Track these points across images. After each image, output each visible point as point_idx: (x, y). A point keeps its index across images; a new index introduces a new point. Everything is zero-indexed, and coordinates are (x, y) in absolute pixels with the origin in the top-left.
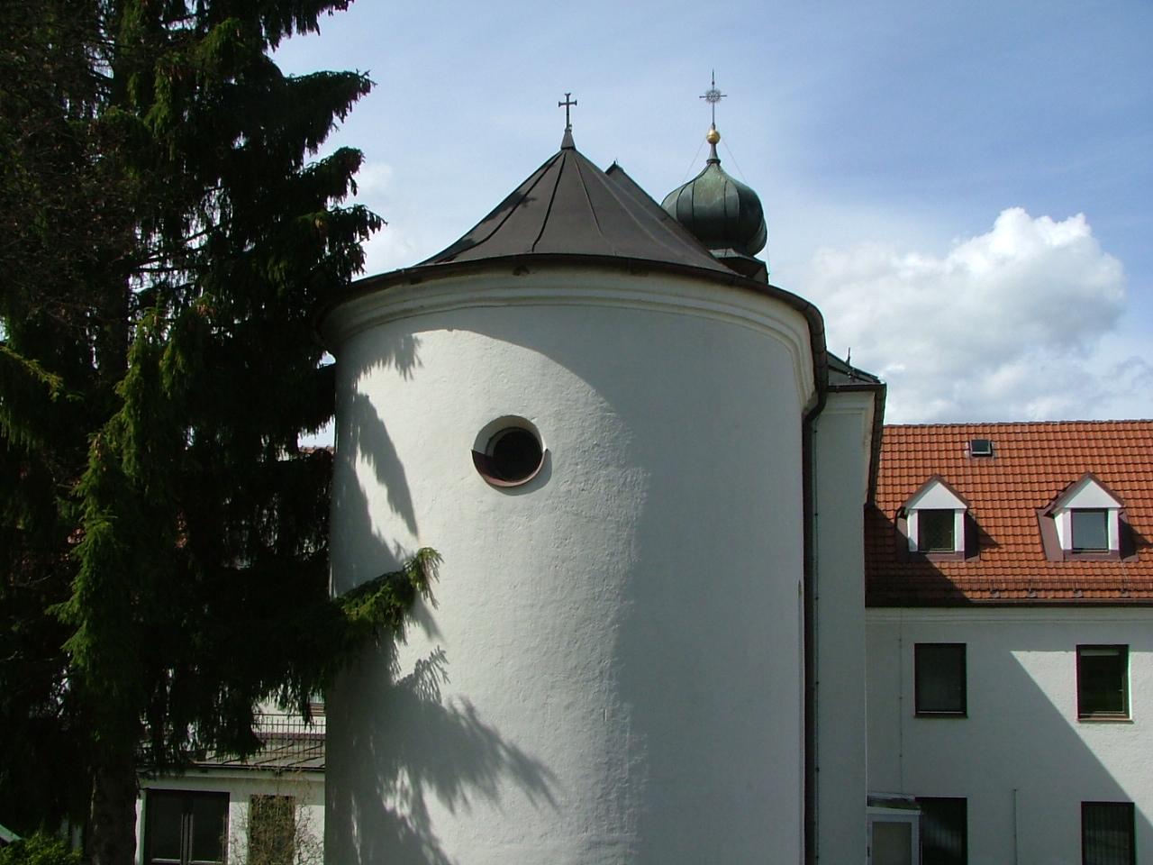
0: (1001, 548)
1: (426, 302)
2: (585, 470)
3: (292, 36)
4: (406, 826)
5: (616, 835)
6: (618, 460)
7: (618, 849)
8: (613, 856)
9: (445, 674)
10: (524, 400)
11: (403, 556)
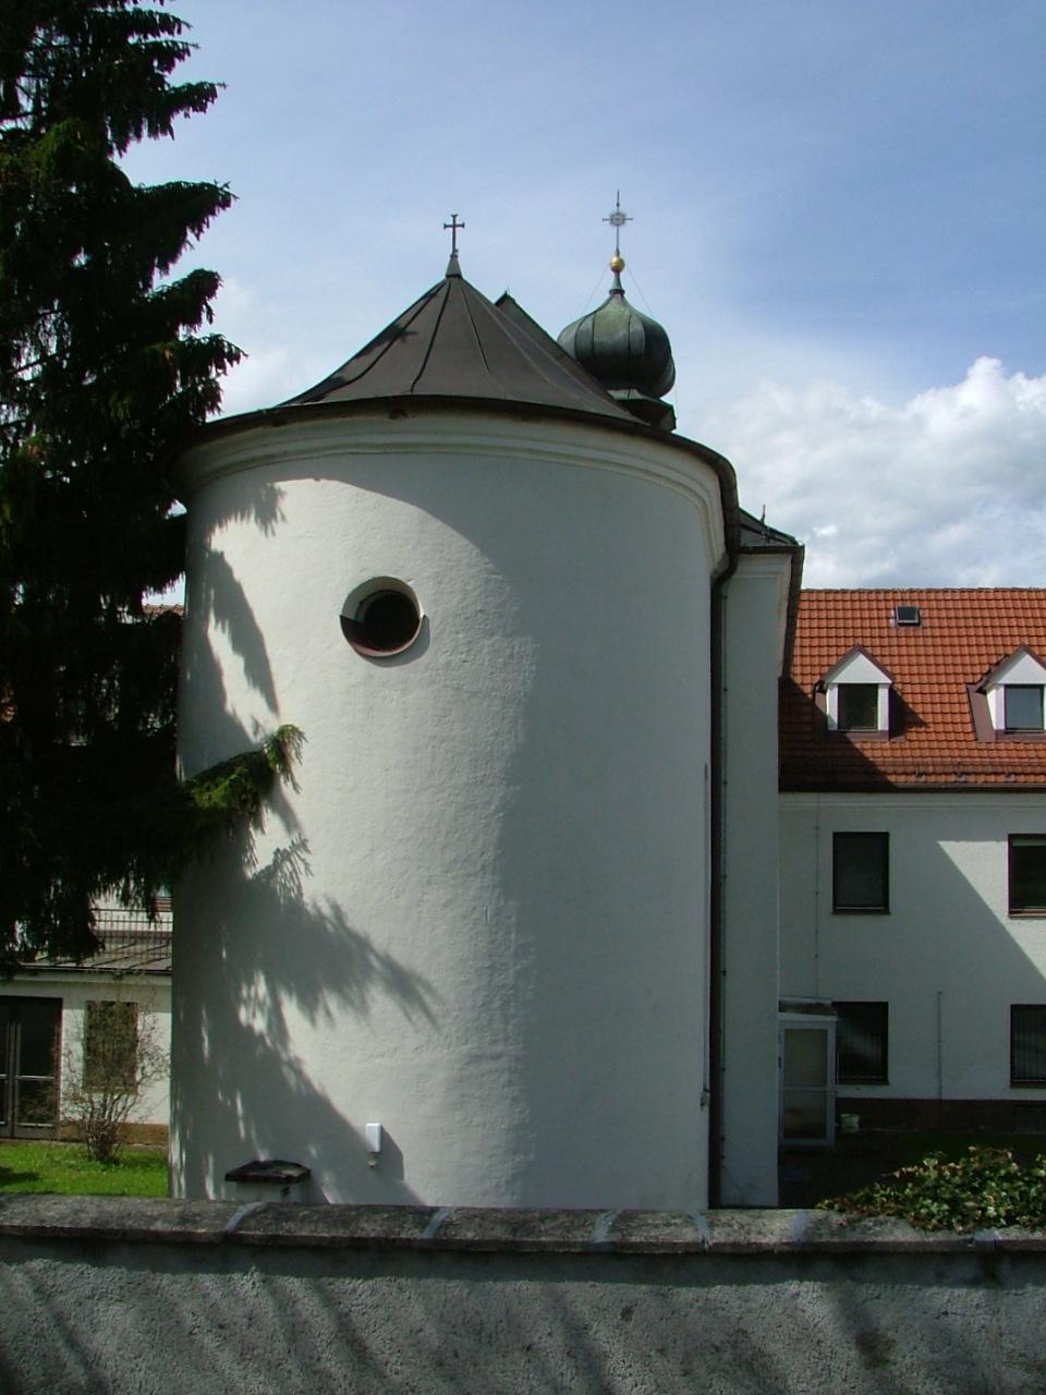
1: (292, 447)
5: (499, 1048)
9: (307, 865)
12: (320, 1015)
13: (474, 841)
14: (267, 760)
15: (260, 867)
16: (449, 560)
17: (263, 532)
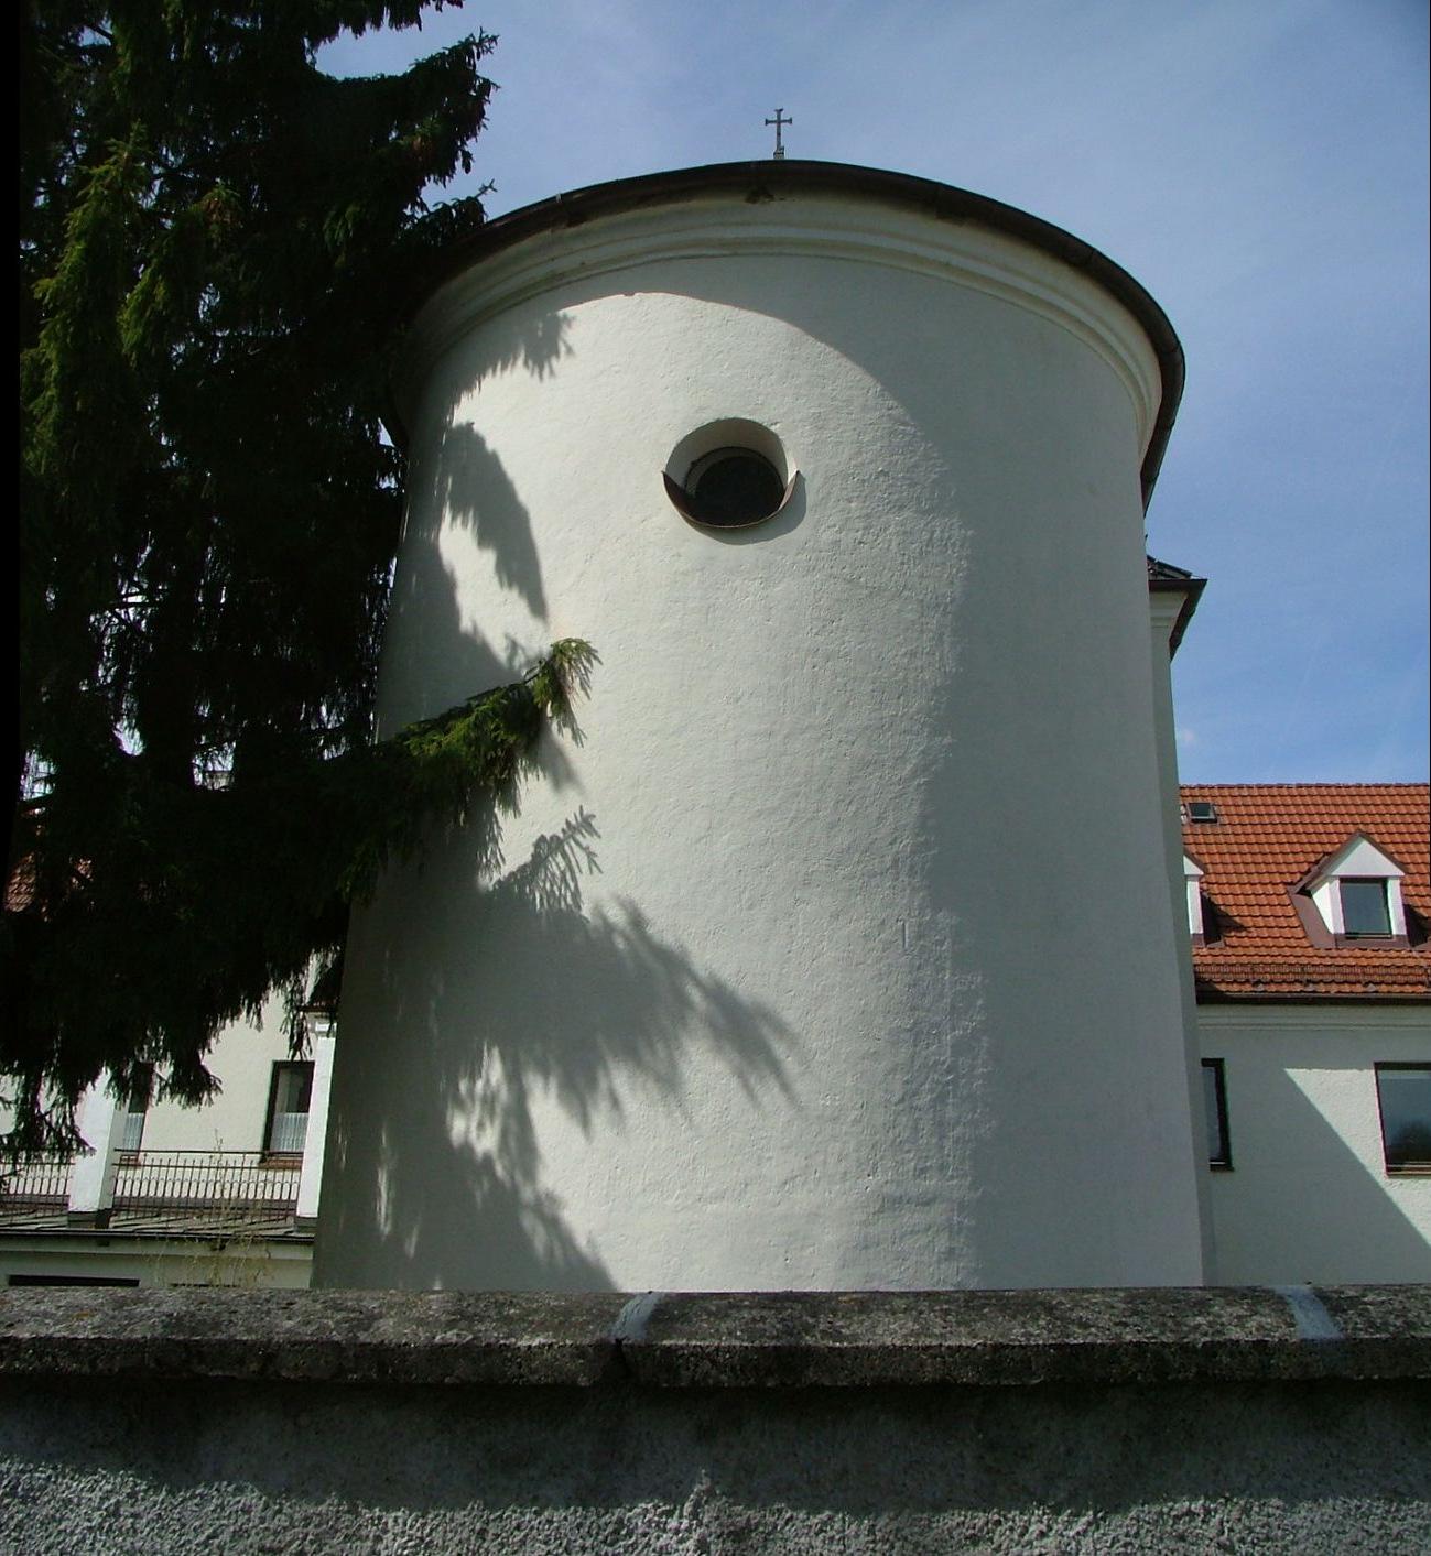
0: (1250, 932)
2: (864, 511)
3: (382, 29)
4: (493, 1174)
5: (931, 1183)
6: (920, 503)
7: (937, 1213)
8: (928, 1229)
9: (591, 855)
10: (759, 395)
11: (520, 659)
12: (600, 1117)
13: (880, 819)
14: (529, 692)
15: (508, 868)
16: (833, 399)
17: (536, 375)
